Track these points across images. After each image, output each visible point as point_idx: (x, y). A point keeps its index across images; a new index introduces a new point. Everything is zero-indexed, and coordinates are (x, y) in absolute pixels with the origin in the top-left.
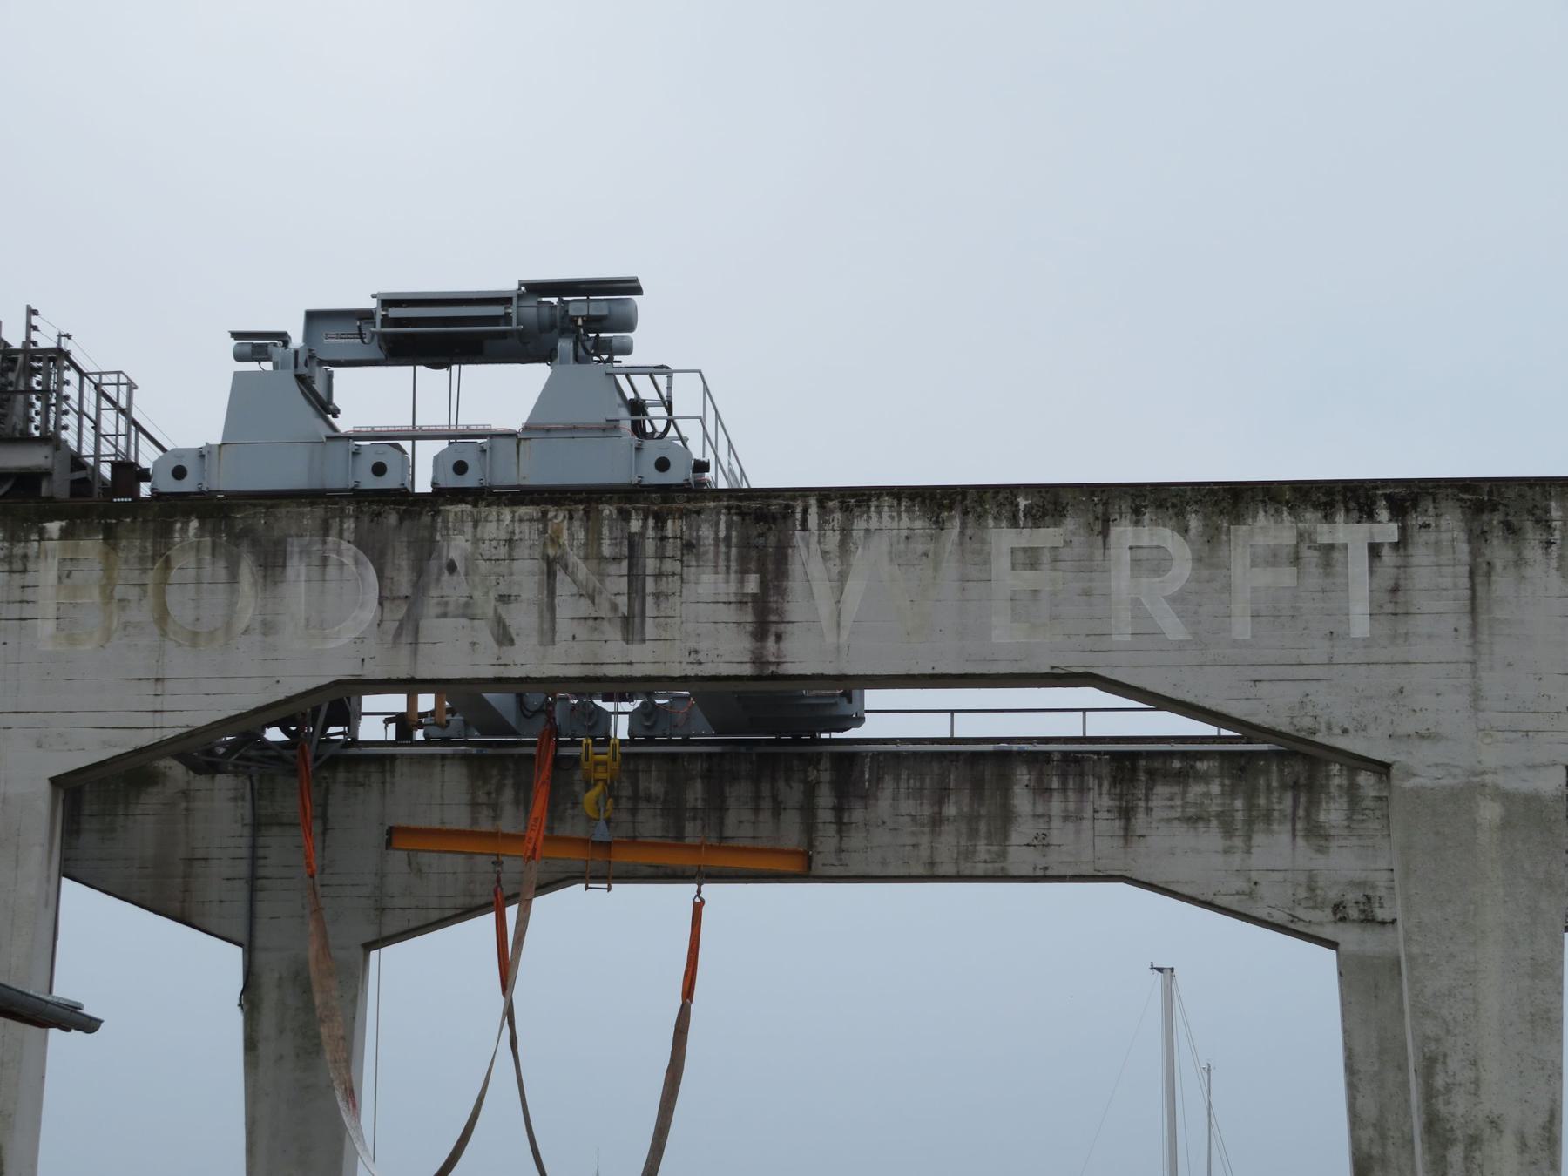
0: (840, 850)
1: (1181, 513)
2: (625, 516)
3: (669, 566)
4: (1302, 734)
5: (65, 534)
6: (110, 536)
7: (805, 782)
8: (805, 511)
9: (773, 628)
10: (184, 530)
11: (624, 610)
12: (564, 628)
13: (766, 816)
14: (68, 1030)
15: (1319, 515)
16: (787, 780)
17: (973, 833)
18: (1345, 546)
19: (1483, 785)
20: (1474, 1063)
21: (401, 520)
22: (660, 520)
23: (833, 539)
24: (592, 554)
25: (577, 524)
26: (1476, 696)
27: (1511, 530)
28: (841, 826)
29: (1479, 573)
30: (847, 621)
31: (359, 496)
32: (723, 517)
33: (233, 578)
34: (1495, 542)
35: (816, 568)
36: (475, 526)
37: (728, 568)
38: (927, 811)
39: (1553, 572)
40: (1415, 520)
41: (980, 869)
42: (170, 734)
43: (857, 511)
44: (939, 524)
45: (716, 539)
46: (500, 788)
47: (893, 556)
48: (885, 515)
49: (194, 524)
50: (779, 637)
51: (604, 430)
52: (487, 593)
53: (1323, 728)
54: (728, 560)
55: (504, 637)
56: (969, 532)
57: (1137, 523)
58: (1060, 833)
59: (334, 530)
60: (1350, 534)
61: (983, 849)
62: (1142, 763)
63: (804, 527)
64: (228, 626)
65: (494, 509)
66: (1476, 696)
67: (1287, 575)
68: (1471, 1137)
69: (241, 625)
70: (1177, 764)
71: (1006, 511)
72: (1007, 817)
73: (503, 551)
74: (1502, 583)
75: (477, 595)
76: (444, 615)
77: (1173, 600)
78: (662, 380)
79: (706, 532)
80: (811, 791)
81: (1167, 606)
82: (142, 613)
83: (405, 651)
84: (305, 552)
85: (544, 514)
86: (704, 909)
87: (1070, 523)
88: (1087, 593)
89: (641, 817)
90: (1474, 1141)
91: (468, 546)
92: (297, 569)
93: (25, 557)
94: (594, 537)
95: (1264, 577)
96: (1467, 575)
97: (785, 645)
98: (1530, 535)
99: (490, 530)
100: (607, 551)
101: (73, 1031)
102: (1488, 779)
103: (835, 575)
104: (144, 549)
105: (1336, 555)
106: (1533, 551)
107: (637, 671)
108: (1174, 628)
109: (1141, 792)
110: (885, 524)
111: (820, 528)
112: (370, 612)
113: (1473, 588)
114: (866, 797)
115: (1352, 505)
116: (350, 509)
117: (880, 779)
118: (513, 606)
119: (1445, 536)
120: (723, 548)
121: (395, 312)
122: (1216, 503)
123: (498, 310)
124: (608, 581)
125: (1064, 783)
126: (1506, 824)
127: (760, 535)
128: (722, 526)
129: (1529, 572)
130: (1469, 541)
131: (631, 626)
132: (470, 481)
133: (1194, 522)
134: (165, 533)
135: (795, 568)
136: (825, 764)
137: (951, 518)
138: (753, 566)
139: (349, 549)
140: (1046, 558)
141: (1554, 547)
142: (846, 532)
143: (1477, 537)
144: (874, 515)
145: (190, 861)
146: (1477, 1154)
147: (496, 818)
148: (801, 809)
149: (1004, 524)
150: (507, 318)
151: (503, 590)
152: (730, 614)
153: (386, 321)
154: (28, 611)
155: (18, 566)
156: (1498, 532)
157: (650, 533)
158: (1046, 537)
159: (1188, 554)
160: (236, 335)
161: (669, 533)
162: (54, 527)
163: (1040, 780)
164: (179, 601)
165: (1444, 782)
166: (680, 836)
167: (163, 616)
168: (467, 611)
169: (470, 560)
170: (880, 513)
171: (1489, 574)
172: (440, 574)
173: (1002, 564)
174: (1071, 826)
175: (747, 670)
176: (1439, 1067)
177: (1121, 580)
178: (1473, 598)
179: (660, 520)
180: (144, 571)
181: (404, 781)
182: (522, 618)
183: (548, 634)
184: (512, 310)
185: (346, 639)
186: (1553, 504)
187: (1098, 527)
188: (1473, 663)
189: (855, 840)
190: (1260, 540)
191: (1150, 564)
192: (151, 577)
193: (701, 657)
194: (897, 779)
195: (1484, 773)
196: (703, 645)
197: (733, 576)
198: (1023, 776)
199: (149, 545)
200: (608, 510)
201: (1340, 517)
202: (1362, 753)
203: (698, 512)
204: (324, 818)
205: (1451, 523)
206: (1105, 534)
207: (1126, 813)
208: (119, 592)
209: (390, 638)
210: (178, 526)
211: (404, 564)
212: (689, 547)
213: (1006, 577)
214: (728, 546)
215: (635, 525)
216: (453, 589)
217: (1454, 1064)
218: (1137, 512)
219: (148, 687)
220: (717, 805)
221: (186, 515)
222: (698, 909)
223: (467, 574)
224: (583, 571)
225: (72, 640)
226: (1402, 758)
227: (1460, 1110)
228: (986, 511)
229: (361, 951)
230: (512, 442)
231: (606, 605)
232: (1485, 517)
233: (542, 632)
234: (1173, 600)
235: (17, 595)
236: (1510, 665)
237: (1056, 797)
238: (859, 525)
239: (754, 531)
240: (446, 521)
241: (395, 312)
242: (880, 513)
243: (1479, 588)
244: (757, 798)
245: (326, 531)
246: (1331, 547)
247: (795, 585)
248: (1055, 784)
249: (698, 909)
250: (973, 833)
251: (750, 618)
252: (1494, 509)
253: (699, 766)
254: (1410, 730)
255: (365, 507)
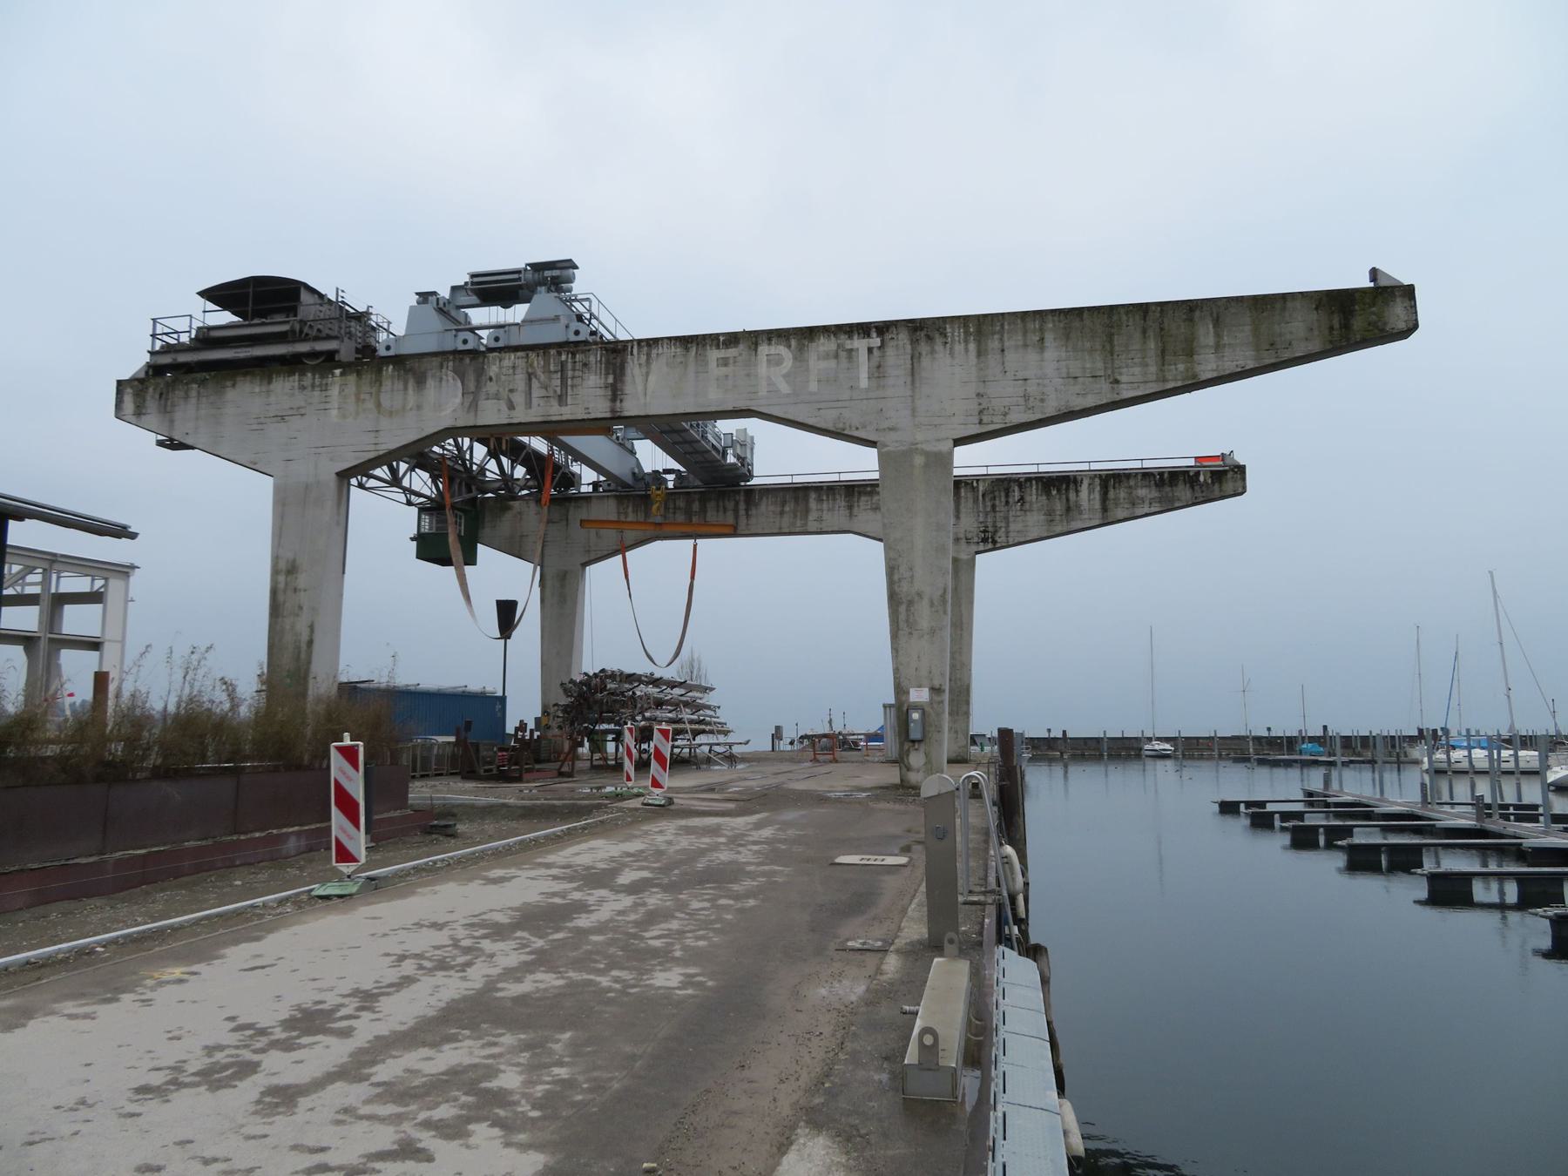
0: (748, 525)
1: (788, 339)
2: (560, 354)
3: (577, 373)
4: (839, 431)
5: (342, 374)
6: (359, 374)
7: (735, 500)
8: (632, 348)
9: (619, 397)
10: (387, 370)
11: (559, 392)
12: (535, 402)
13: (721, 513)
14: (120, 538)
15: (847, 336)
16: (729, 500)
17: (795, 516)
18: (858, 349)
19: (917, 449)
20: (911, 569)
21: (471, 360)
22: (574, 354)
23: (643, 358)
24: (547, 371)
25: (540, 358)
26: (914, 411)
27: (929, 338)
28: (748, 516)
29: (915, 358)
30: (649, 391)
31: (455, 352)
32: (599, 352)
33: (406, 388)
34: (922, 344)
35: (637, 371)
36: (500, 361)
37: (601, 373)
38: (779, 509)
39: (947, 355)
40: (888, 336)
41: (797, 530)
42: (381, 453)
43: (653, 346)
44: (687, 349)
45: (596, 361)
46: (628, 507)
47: (667, 364)
48: (665, 347)
49: (391, 367)
50: (621, 401)
51: (554, 320)
52: (504, 389)
53: (848, 427)
54: (601, 369)
55: (511, 406)
56: (699, 353)
57: (770, 344)
58: (826, 516)
59: (445, 366)
60: (860, 344)
61: (799, 523)
62: (856, 489)
63: (632, 354)
64: (404, 408)
65: (507, 354)
66: (914, 411)
67: (832, 363)
68: (910, 601)
69: (409, 408)
70: (869, 489)
71: (715, 342)
72: (807, 511)
73: (511, 371)
74: (926, 362)
75: (501, 390)
76: (488, 399)
77: (785, 376)
78: (586, 304)
79: (592, 359)
80: (737, 504)
81: (781, 379)
82: (370, 405)
83: (472, 414)
84: (433, 376)
85: (527, 355)
86: (698, 546)
87: (741, 346)
88: (748, 375)
89: (677, 515)
90: (910, 603)
91: (497, 370)
92: (431, 383)
93: (327, 384)
94: (547, 363)
95: (823, 365)
96: (910, 358)
97: (624, 404)
98: (937, 340)
99: (506, 363)
100: (552, 368)
101: (27, 520)
102: (919, 446)
103: (644, 373)
104: (371, 378)
105: (854, 353)
106: (939, 347)
107: (564, 418)
108: (784, 388)
109: (856, 499)
110: (666, 351)
111: (638, 354)
112: (458, 400)
113: (912, 364)
114: (757, 505)
115: (861, 331)
116: (451, 357)
117: (762, 498)
118: (515, 394)
119: (901, 343)
120: (599, 365)
121: (476, 280)
122: (803, 334)
123: (516, 276)
124: (553, 381)
125: (828, 497)
126: (927, 465)
127: (615, 358)
128: (599, 355)
129: (937, 356)
130: (911, 344)
131: (562, 399)
132: (500, 344)
133: (793, 343)
134: (380, 371)
135: (628, 371)
136: (742, 494)
137: (692, 347)
138: (611, 372)
139: (451, 374)
140: (731, 361)
141: (948, 345)
142: (649, 355)
143: (914, 342)
144: (660, 348)
145: (522, 536)
146: (912, 608)
147: (626, 518)
148: (734, 510)
149: (714, 348)
150: (520, 279)
151: (511, 387)
152: (601, 392)
153: (473, 283)
154: (328, 406)
155: (324, 388)
156: (923, 338)
157: (570, 360)
158: (731, 352)
159: (791, 356)
160: (417, 294)
161: (577, 360)
162: (338, 372)
163: (819, 497)
164: (386, 400)
165: (899, 449)
166: (691, 521)
167: (379, 405)
168: (497, 397)
169: (498, 376)
170: (662, 347)
171: (920, 358)
172: (486, 382)
173: (713, 364)
174: (830, 513)
175: (608, 415)
176: (896, 571)
177: (763, 369)
178: (913, 369)
179: (574, 354)
180: (371, 388)
181: (595, 506)
182: (519, 398)
183: (529, 404)
184: (522, 275)
185: (449, 411)
186: (948, 326)
187: (753, 347)
188: (912, 396)
189: (753, 521)
190: (821, 349)
191: (775, 361)
192: (374, 390)
193: (590, 411)
194: (767, 498)
195: (917, 444)
196: (591, 406)
197: (603, 376)
198: (813, 495)
199: (374, 376)
200: (553, 352)
201: (856, 337)
202: (865, 437)
203: (589, 350)
204: (567, 520)
205: (903, 337)
206: (756, 350)
207: (850, 508)
208: (362, 396)
209: (466, 409)
210: (385, 368)
211: (472, 378)
212: (585, 365)
213: (714, 370)
214: (601, 364)
215: (564, 357)
216: (491, 388)
217: (902, 569)
218: (770, 339)
219: (373, 434)
220: (703, 510)
221: (387, 364)
222: (695, 546)
223: (497, 381)
224: (542, 377)
225: (344, 417)
226: (882, 439)
227: (905, 590)
228: (706, 343)
229: (580, 567)
230: (517, 328)
231: (552, 392)
232: (918, 333)
233: (526, 404)
234: (785, 376)
235: (324, 400)
236: (928, 396)
237: (825, 502)
238: (654, 352)
239: (612, 356)
240: (488, 359)
241: (476, 280)
242: (662, 347)
243: (915, 364)
244: (718, 506)
245: (441, 367)
246: (852, 350)
247: (628, 378)
248: (825, 498)
249: (695, 546)
250: (795, 516)
251: (610, 393)
252: (922, 330)
253: (697, 496)
254: (885, 427)
255: (457, 356)
